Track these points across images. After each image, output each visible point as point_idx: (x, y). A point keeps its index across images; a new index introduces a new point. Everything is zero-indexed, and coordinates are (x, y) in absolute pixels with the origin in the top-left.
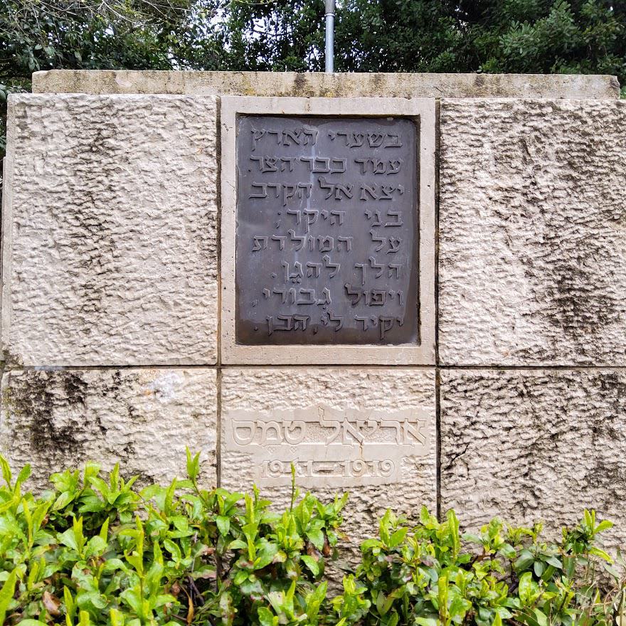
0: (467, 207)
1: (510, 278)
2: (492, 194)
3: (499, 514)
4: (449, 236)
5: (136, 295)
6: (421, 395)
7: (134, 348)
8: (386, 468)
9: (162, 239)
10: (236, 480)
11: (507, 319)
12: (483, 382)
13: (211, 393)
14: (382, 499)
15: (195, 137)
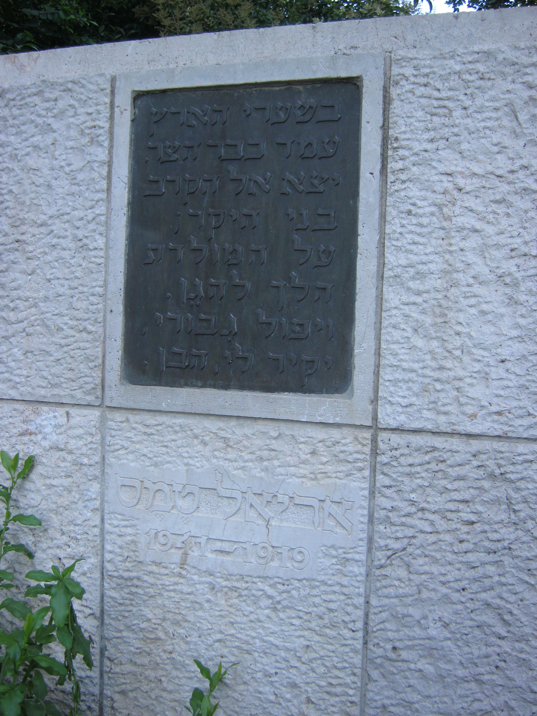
0: (425, 203)
1: (485, 307)
2: (461, 182)
3: (449, 639)
4: (399, 244)
5: (21, 316)
6: (350, 466)
7: (17, 379)
8: (299, 558)
9: (47, 250)
10: (121, 547)
11: (477, 367)
12: (436, 454)
13: (94, 440)
14: (292, 597)
15: (85, 125)
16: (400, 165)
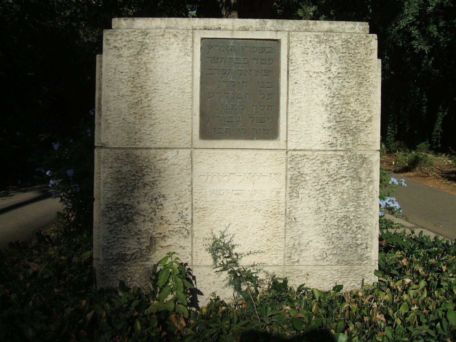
16: (293, 68)
